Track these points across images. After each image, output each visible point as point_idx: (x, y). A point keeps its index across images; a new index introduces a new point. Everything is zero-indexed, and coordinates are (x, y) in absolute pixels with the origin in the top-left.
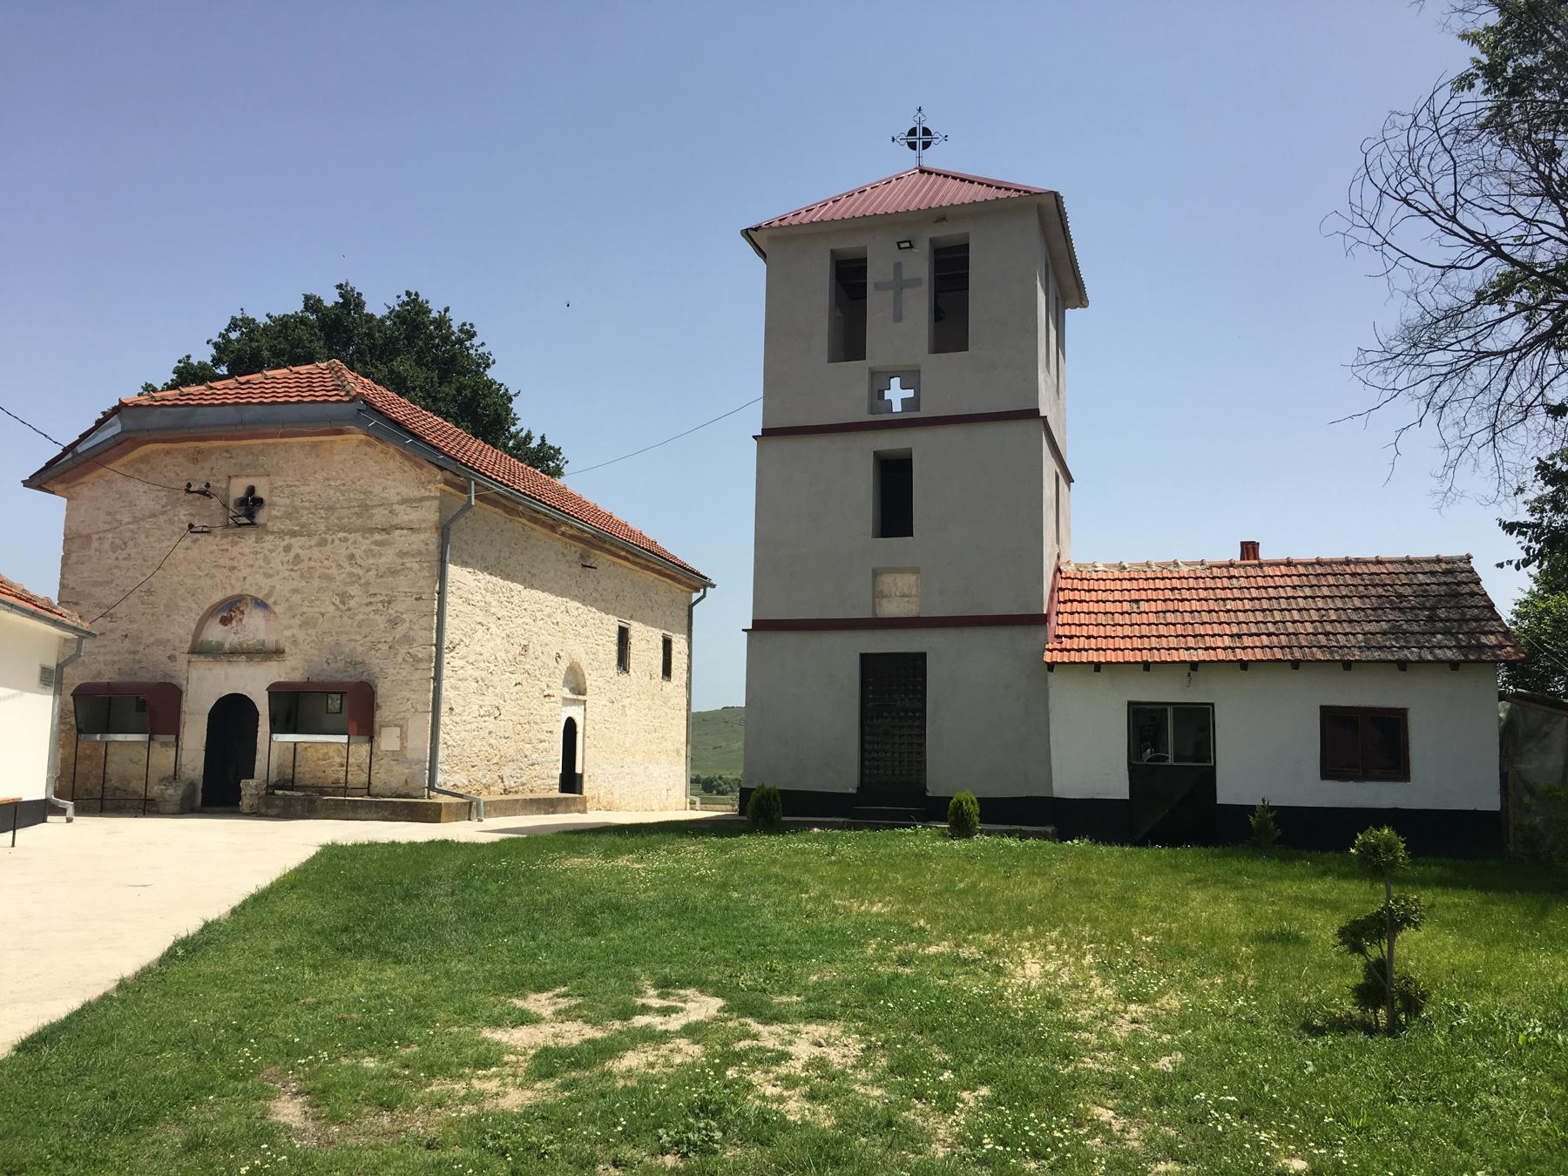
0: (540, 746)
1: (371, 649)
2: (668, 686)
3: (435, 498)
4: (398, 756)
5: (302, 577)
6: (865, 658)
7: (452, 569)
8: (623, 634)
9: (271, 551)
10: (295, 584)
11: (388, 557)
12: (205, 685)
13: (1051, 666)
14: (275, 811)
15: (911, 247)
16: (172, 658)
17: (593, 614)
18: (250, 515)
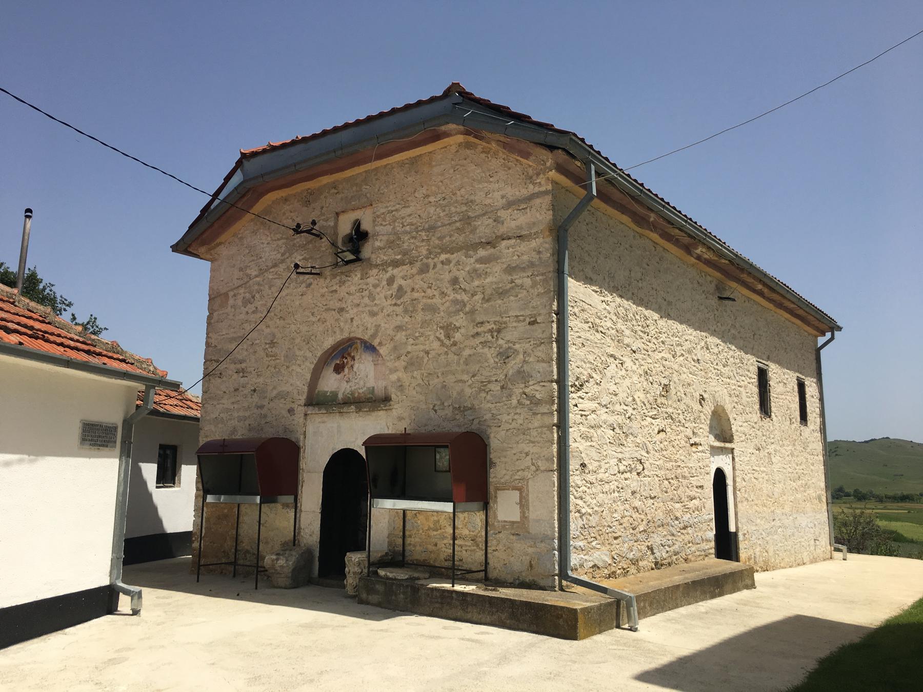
0: (692, 504)
1: (480, 390)
3: (546, 193)
4: (520, 529)
5: (406, 311)
7: (574, 287)
8: (762, 376)
9: (375, 286)
10: (398, 321)
11: (495, 276)
12: (329, 437)
14: (374, 598)
16: (291, 411)
17: (732, 353)
18: (356, 251)
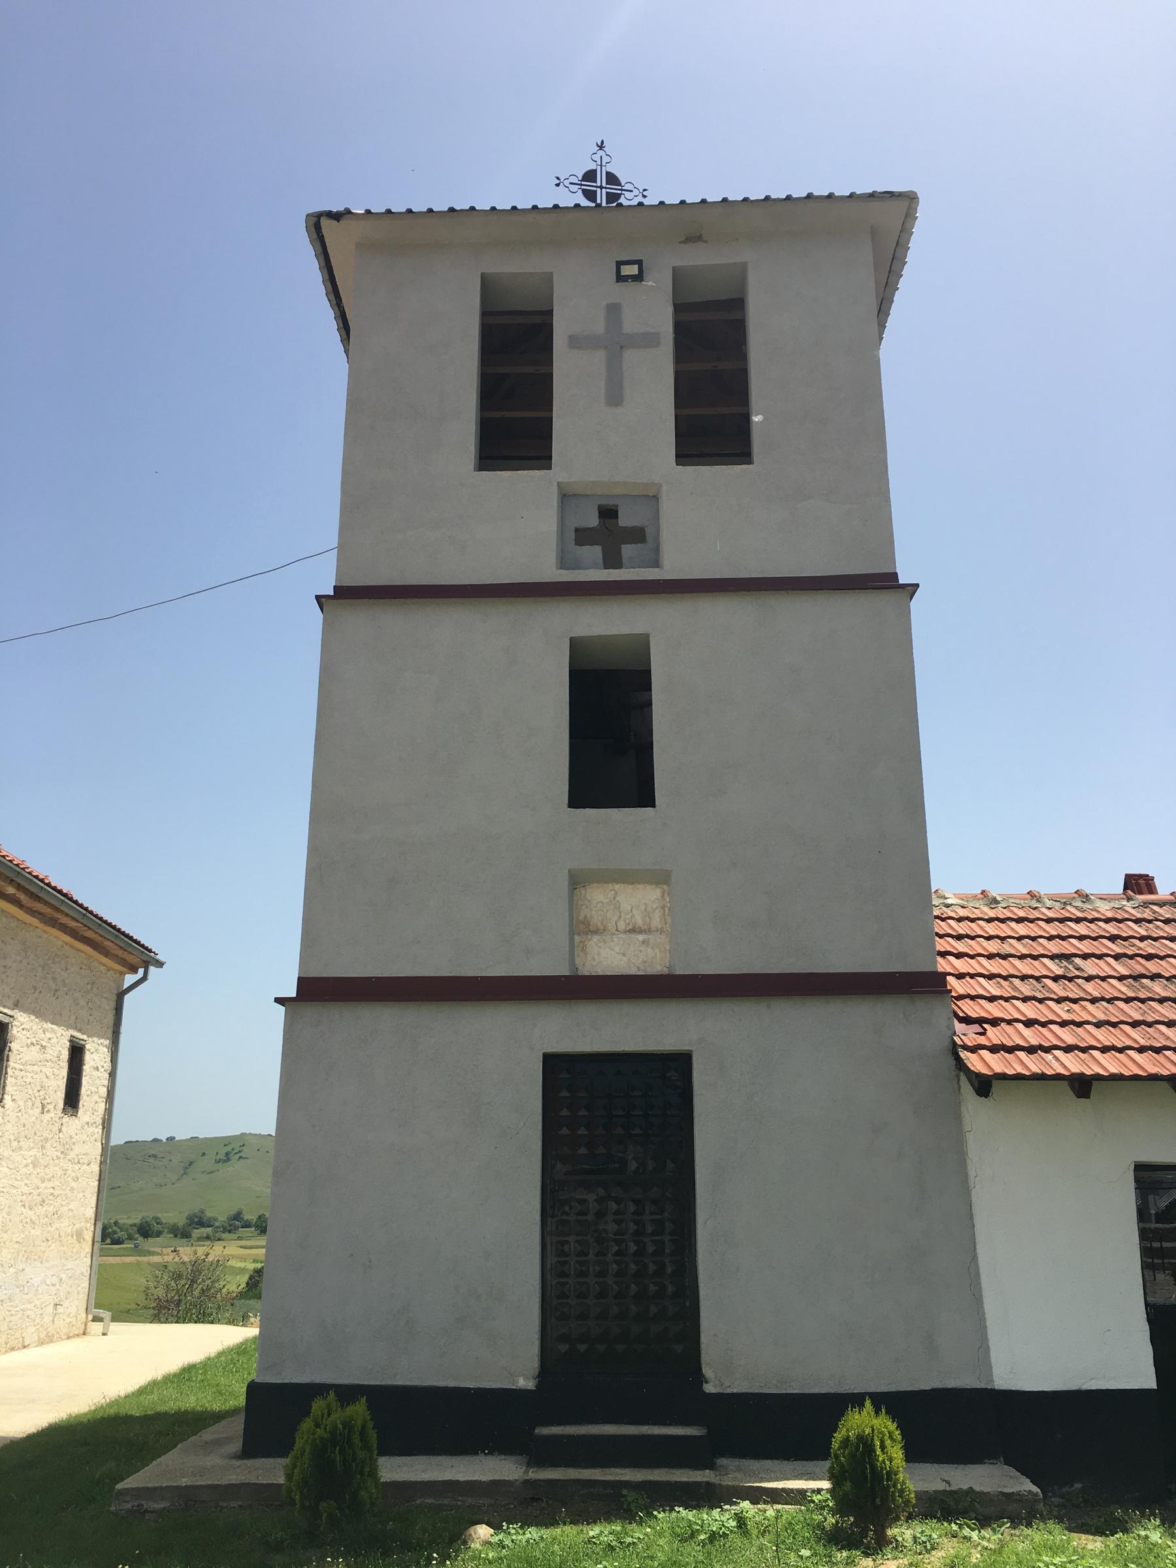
2: (72, 1125)
6: (553, 1064)
13: (984, 1085)
15: (639, 278)
